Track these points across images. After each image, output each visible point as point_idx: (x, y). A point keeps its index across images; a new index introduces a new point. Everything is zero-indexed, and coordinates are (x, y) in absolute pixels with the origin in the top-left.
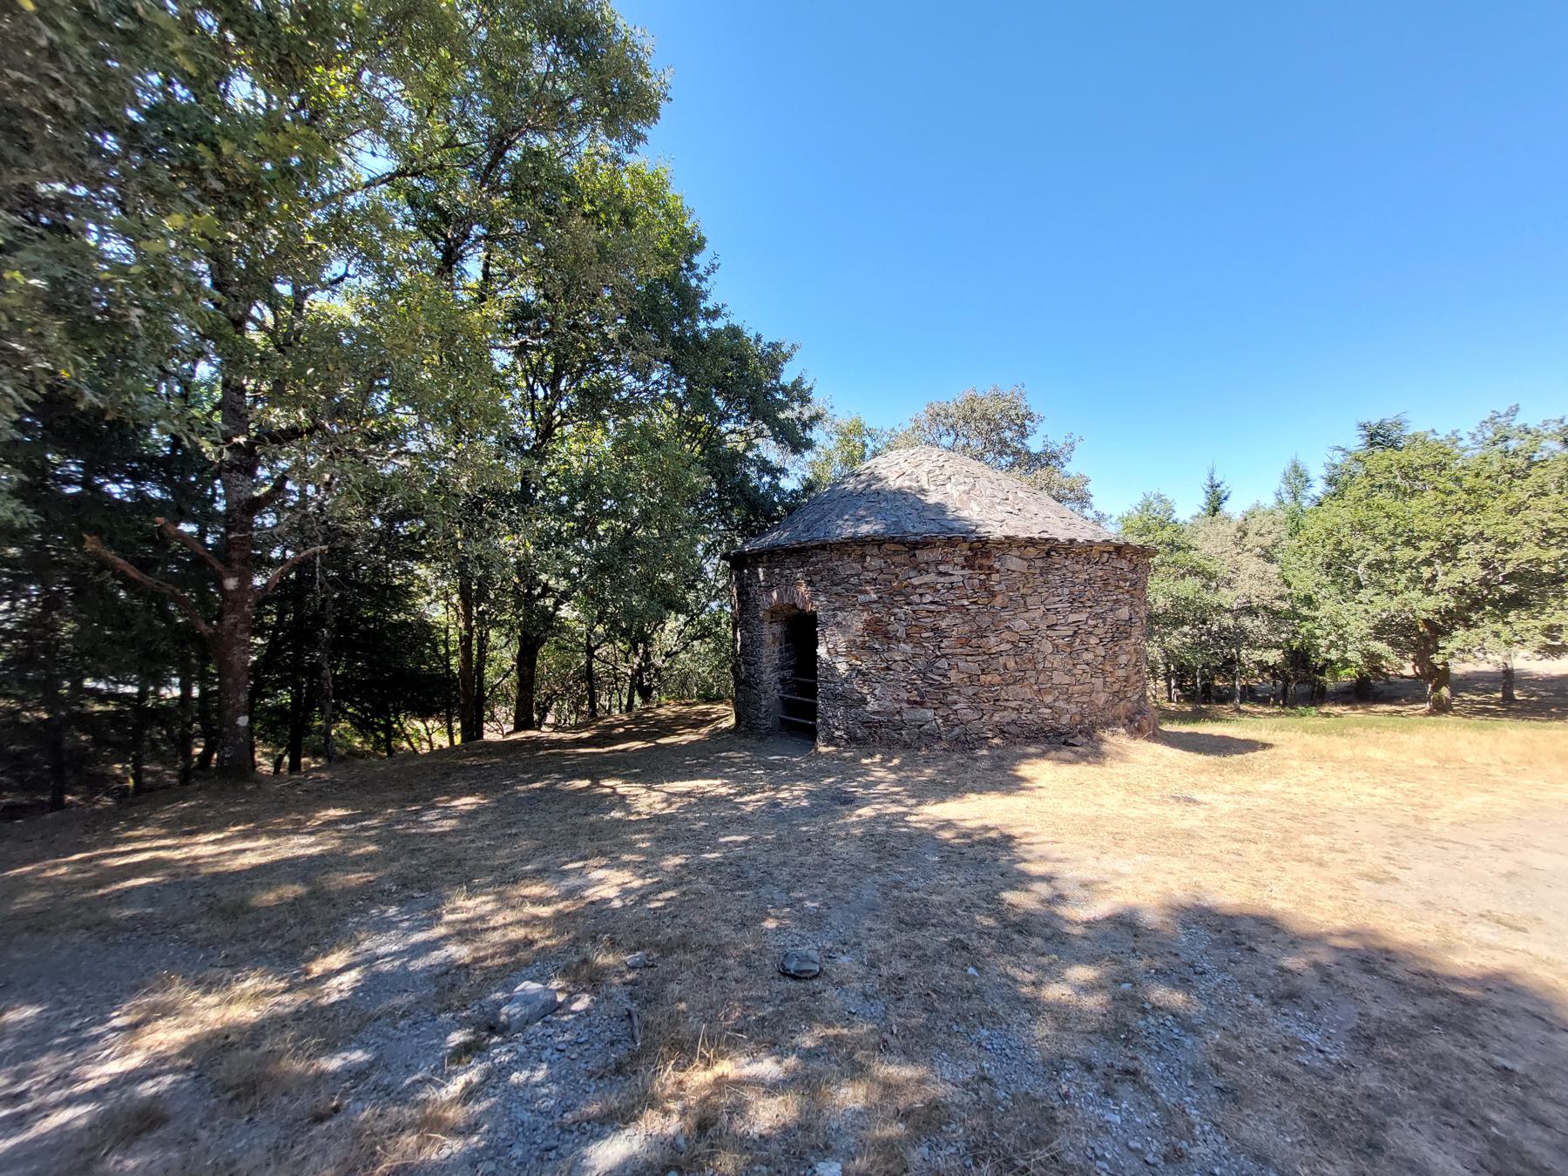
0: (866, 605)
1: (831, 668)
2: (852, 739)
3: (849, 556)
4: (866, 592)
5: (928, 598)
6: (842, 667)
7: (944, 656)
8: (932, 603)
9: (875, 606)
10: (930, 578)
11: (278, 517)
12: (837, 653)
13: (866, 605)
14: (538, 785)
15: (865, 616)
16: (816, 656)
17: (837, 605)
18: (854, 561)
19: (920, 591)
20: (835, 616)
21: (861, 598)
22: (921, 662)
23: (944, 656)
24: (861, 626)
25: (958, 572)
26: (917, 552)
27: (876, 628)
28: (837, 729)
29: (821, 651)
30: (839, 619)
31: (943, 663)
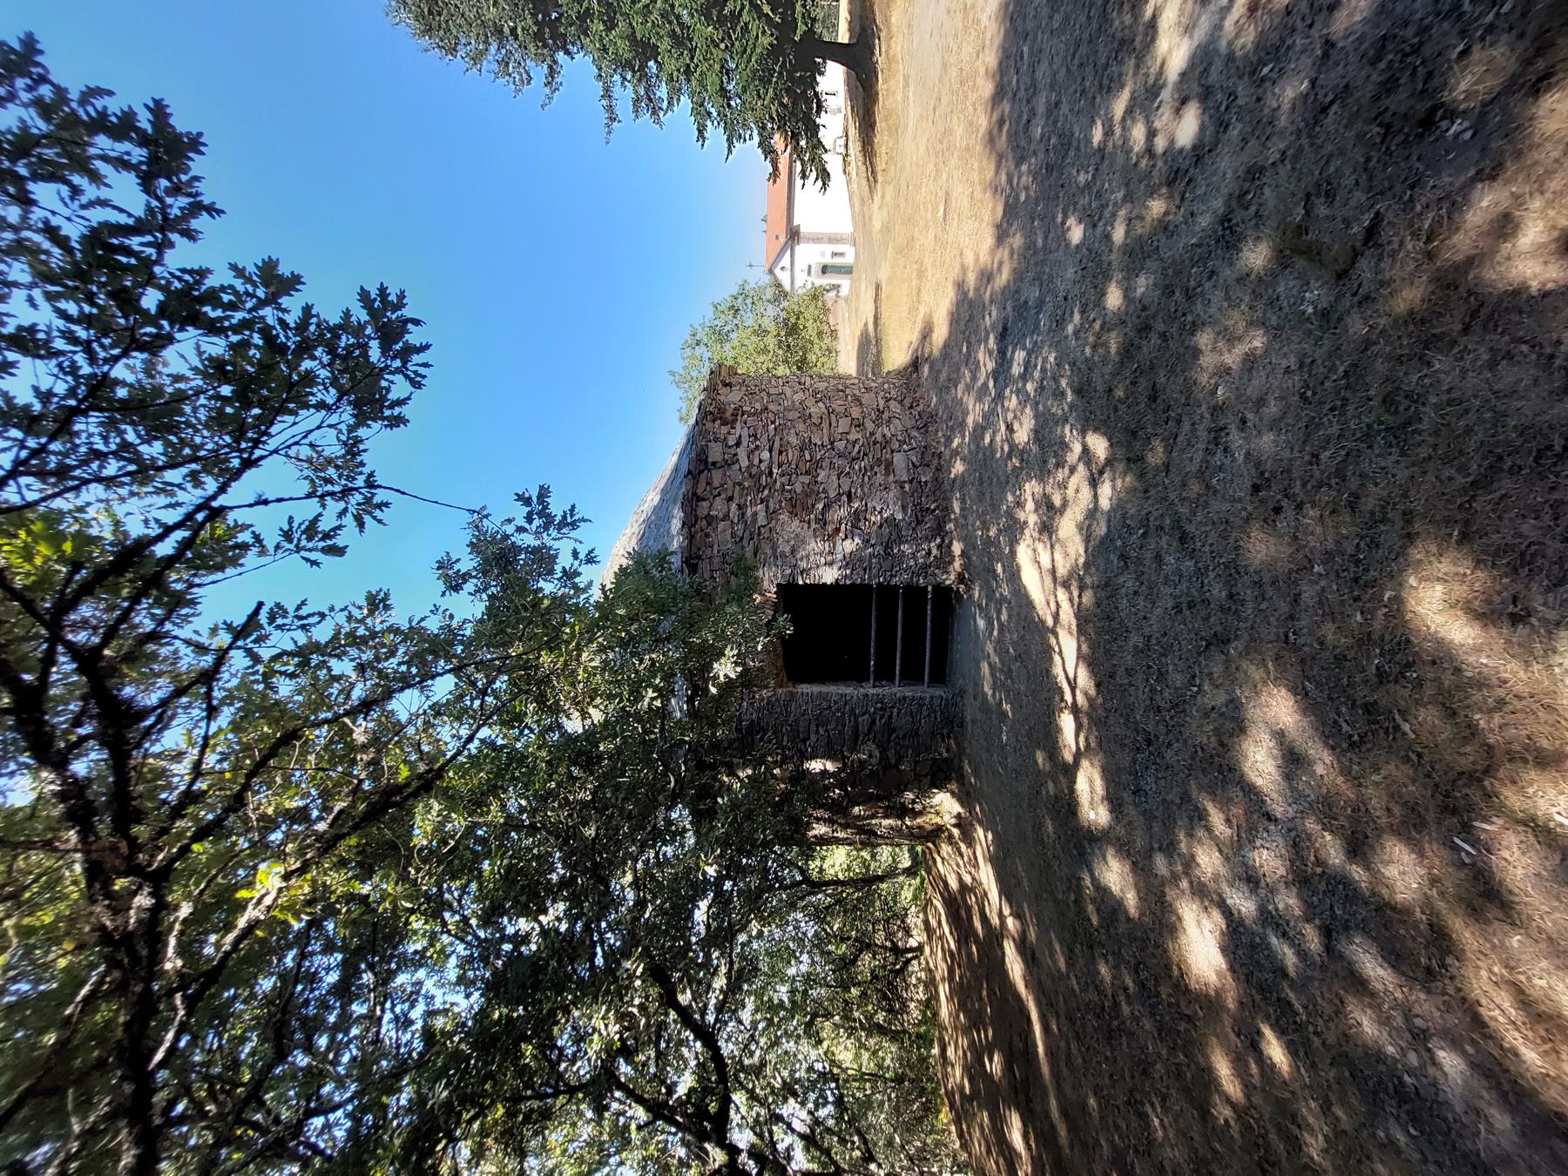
0: (771, 515)
1: (850, 562)
2: (939, 530)
3: (707, 535)
4: (755, 514)
5: (765, 455)
6: (849, 546)
7: (832, 443)
8: (770, 451)
9: (772, 506)
10: (742, 453)
11: (1024, 349)
12: (831, 553)
13: (771, 515)
14: (1053, 1103)
15: (784, 517)
16: (836, 587)
17: (769, 552)
18: (715, 529)
19: (756, 461)
20: (783, 555)
21: (761, 520)
22: (839, 462)
23: (832, 443)
24: (796, 522)
25: (738, 431)
26: (710, 460)
27: (798, 506)
28: (929, 553)
29: (829, 576)
30: (787, 549)
31: (840, 445)
